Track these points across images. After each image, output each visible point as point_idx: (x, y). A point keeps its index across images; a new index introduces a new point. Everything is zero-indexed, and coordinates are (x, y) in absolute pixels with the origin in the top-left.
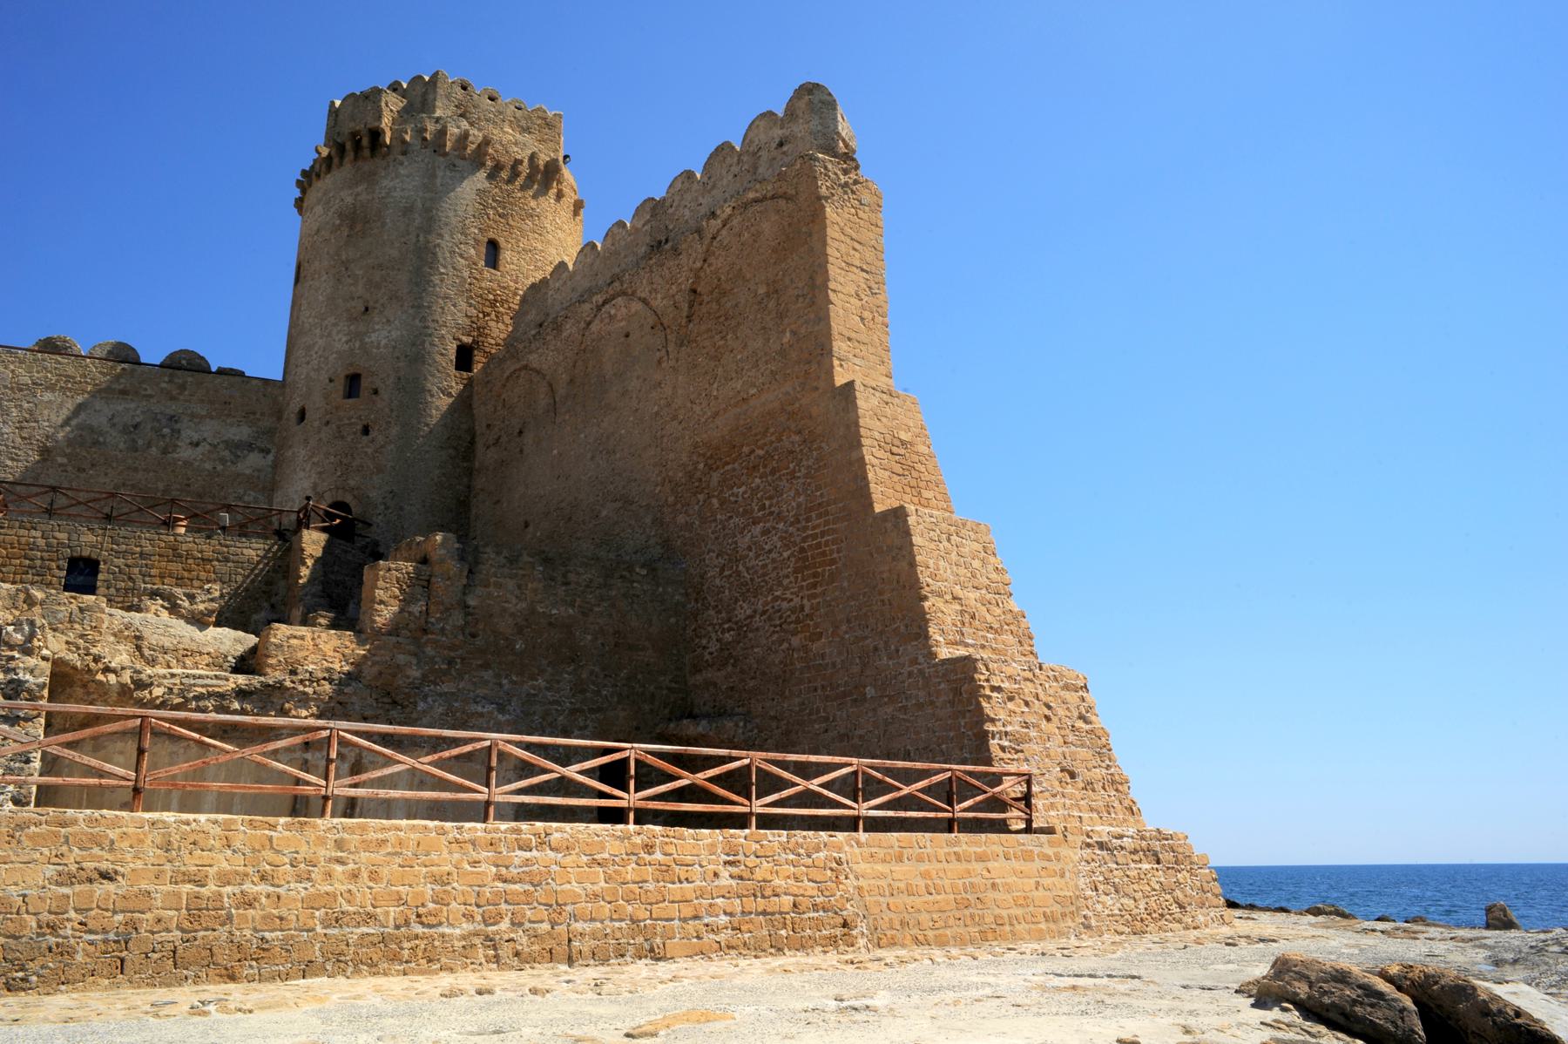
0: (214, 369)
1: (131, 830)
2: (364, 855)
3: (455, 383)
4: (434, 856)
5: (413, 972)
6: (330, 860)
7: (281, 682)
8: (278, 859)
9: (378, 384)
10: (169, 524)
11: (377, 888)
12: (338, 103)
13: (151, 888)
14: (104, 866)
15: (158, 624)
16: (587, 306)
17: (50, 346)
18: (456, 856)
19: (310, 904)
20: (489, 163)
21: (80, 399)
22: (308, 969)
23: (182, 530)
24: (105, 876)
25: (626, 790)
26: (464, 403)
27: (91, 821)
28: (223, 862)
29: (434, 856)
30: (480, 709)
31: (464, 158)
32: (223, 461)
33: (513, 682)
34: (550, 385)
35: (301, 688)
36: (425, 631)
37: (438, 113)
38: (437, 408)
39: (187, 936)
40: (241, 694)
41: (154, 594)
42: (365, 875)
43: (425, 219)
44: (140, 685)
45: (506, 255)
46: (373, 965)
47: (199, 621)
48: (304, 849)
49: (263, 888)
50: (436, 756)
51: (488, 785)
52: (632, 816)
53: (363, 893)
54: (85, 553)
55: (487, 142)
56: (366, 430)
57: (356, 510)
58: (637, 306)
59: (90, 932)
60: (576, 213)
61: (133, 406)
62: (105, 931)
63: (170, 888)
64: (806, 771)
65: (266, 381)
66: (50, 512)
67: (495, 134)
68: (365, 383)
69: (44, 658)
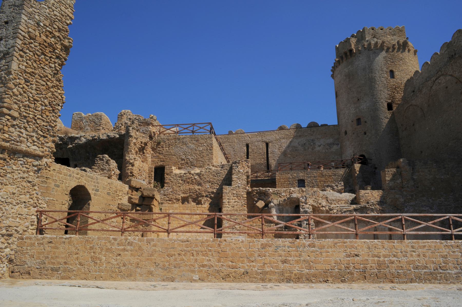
1: (360, 244)
2: (420, 250)
3: (388, 114)
4: (440, 250)
5: (442, 283)
6: (411, 251)
7: (365, 206)
8: (397, 251)
10: (319, 168)
11: (426, 259)
12: (337, 46)
13: (368, 258)
14: (356, 253)
15: (330, 193)
16: (429, 82)
17: (281, 128)
18: (447, 250)
19: (409, 263)
20: (385, 48)
21: (290, 140)
22: (412, 281)
23: (322, 169)
24: (356, 255)
26: (392, 120)
27: (350, 242)
28: (383, 252)
29: (440, 250)
30: (424, 209)
31: (378, 49)
32: (327, 149)
33: (433, 200)
34: (421, 109)
35: (371, 207)
36: (403, 188)
37: (367, 39)
38: (385, 123)
39: (379, 271)
40: (355, 210)
41: (328, 186)
42: (422, 255)
43: (370, 69)
44: (331, 210)
45: (396, 73)
46: (429, 281)
47: (340, 192)
48: (403, 248)
49: (394, 259)
50: (433, 222)
51: (450, 229)
53: (423, 261)
54: (301, 178)
55: (383, 42)
56: (365, 133)
57: (367, 156)
58: (448, 78)
59: (356, 269)
60: (415, 54)
62: (359, 269)
63: (372, 258)
65: (334, 125)
66: (291, 169)
67: (385, 39)
68: (362, 120)
69: (309, 205)
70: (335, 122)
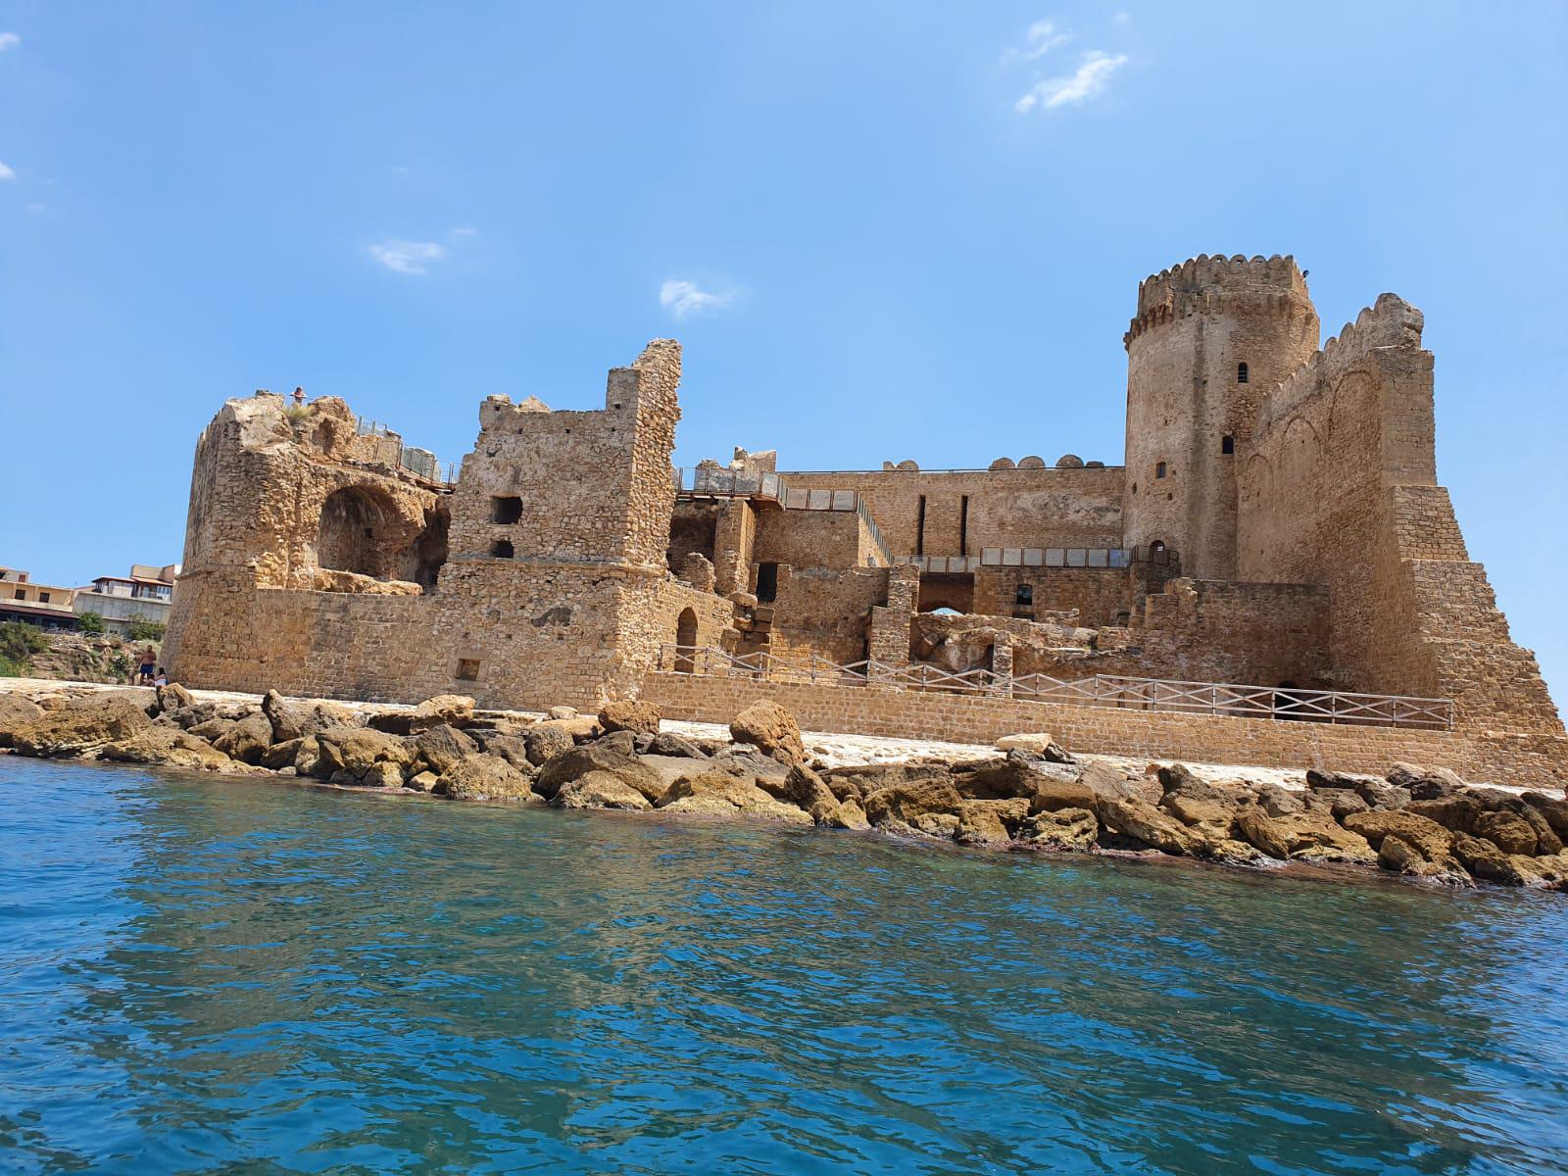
16: (1282, 422)
19: (1088, 732)
25: (1270, 706)
32: (1093, 519)
45: (1253, 372)
58: (1306, 425)
64: (1363, 701)
68: (1168, 468)
70: (1119, 461)
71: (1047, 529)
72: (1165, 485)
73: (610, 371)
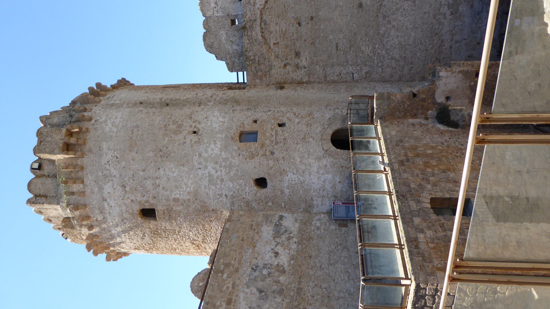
0: (208, 267)
9: (250, 120)
32: (289, 239)
52: (470, 193)
61: (242, 295)
71: (299, 290)
72: (267, 132)
73: (45, 186)
